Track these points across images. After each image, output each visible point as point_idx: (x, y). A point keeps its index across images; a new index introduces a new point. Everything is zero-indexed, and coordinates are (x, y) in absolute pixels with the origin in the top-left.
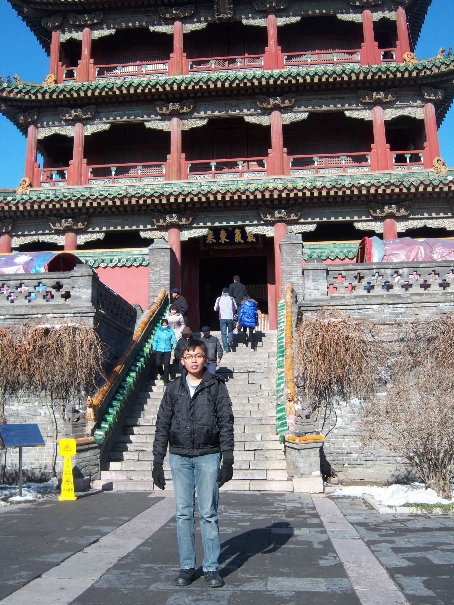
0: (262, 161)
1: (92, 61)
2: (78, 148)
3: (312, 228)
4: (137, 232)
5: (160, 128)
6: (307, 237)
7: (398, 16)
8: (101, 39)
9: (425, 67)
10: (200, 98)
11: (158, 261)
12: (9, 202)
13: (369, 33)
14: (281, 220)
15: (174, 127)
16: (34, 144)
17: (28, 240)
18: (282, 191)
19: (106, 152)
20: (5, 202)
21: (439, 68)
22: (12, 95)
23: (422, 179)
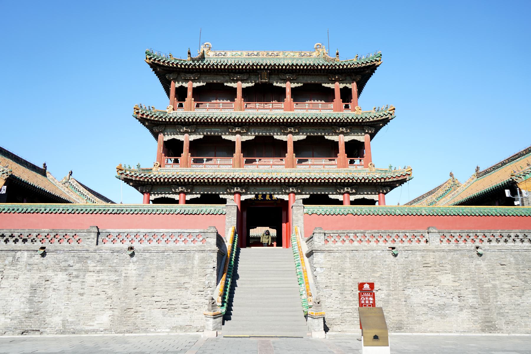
1: (193, 99)
2: (186, 147)
3: (308, 196)
6: (306, 202)
7: (353, 86)
8: (198, 87)
9: (366, 117)
11: (230, 212)
12: (152, 177)
13: (337, 94)
14: (293, 192)
15: (238, 139)
16: (162, 144)
17: (157, 196)
18: (294, 179)
19: (200, 150)
20: (149, 177)
21: (373, 118)
22: (152, 118)
23: (363, 176)
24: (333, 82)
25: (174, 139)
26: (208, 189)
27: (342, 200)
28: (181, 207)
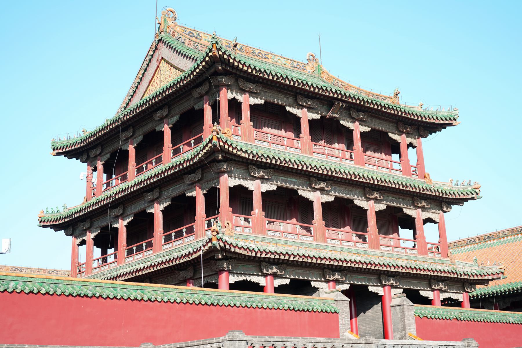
0: (248, 219)
4: (309, 282)
5: (410, 214)
10: (285, 171)
11: (343, 310)
24: (401, 133)
25: (240, 186)
26: (300, 271)
27: (264, 284)
28: (268, 299)
